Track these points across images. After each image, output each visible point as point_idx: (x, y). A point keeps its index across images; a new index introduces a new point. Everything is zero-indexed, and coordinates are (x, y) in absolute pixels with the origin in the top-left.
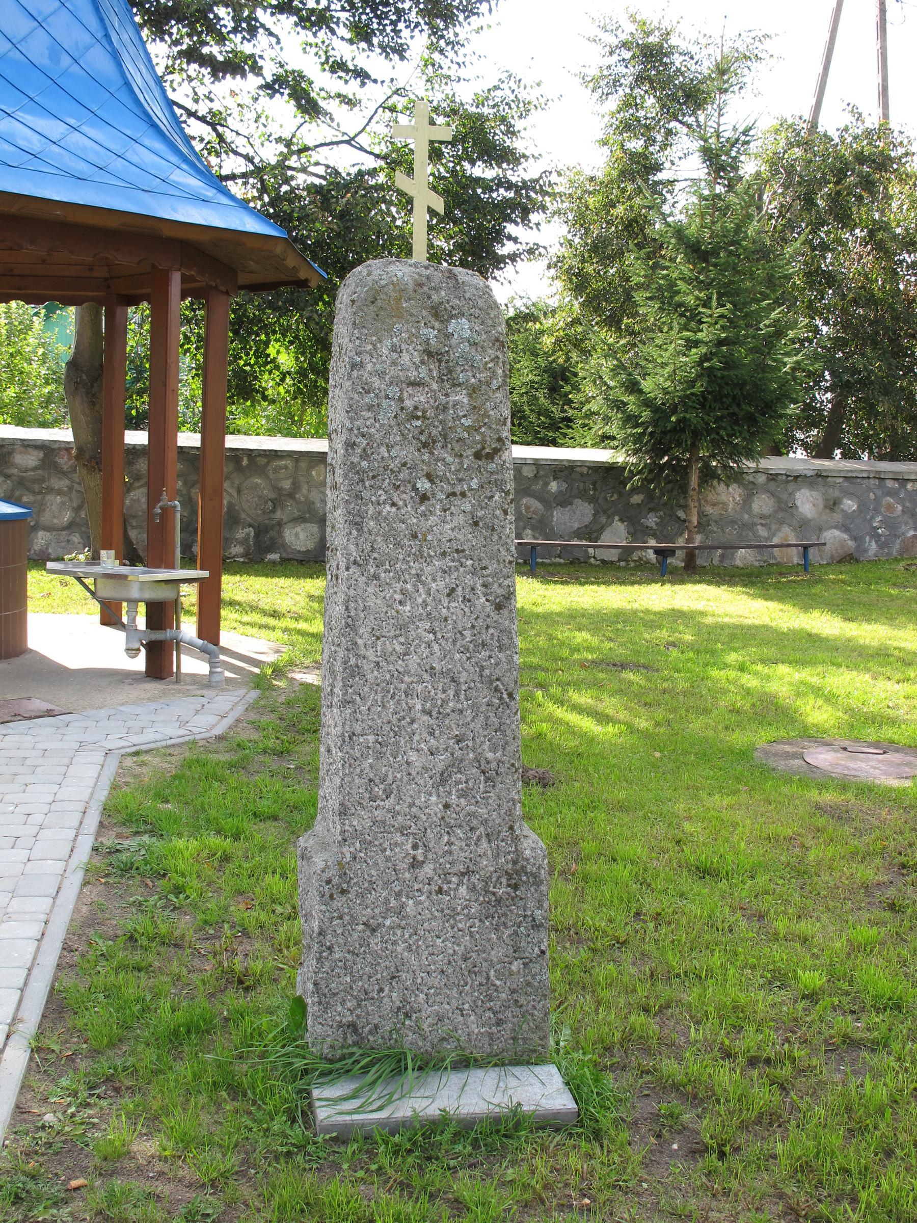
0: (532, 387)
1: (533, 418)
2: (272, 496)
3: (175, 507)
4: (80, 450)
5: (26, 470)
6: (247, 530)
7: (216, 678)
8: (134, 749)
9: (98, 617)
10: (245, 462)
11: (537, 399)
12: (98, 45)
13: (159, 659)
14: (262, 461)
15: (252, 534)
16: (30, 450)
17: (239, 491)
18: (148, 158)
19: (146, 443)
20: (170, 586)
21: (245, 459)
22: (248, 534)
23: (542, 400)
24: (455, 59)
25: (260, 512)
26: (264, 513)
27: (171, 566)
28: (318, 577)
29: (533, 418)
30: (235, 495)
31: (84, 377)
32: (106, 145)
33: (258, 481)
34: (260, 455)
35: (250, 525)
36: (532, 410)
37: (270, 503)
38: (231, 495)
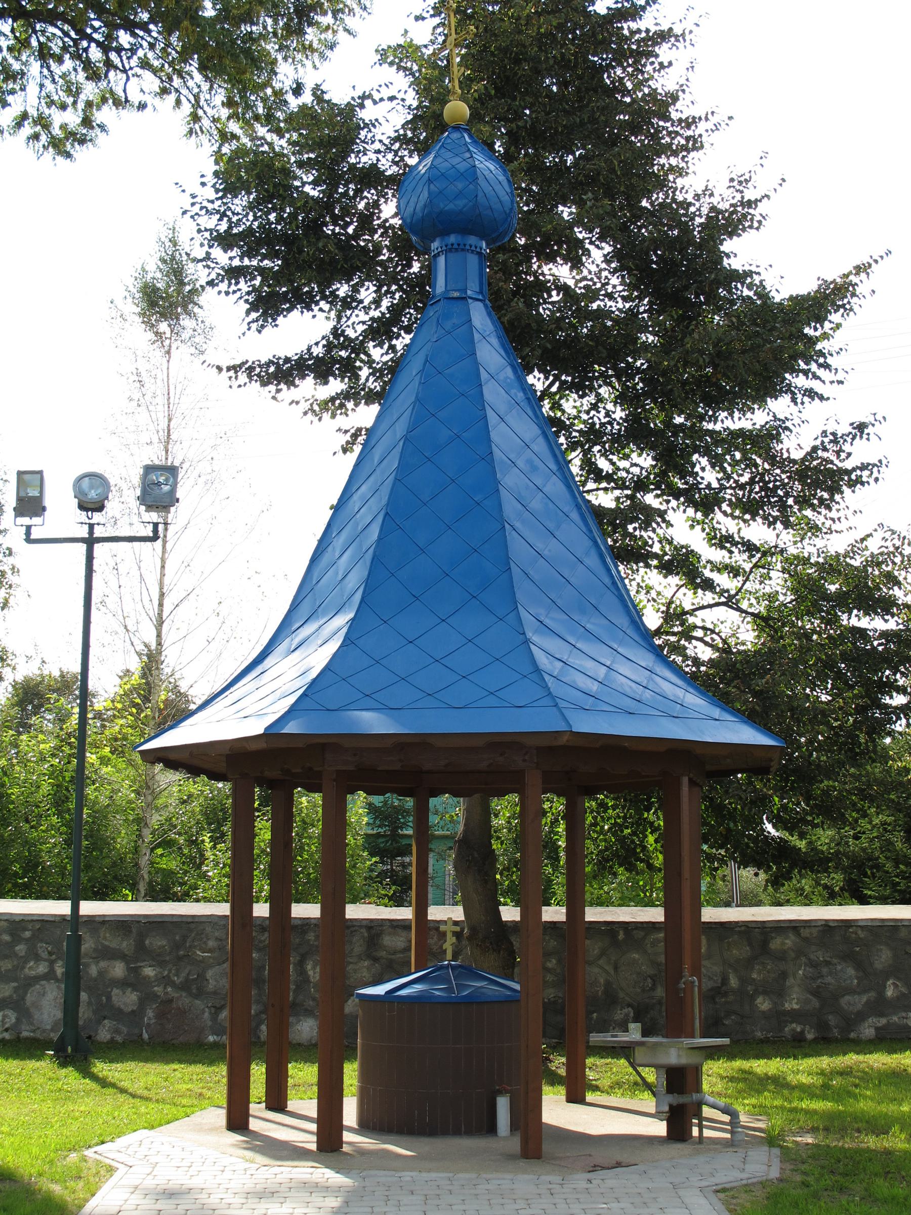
0: (885, 829)
1: (889, 866)
2: (651, 972)
3: (693, 982)
4: (473, 929)
5: (395, 953)
6: (626, 1010)
7: (738, 1137)
8: (719, 1187)
9: (564, 1098)
10: (621, 936)
11: (892, 844)
12: (609, 592)
13: (680, 1121)
14: (639, 934)
15: (632, 1014)
16: (399, 931)
17: (616, 968)
18: (667, 688)
19: (518, 919)
20: (696, 1051)
21: (621, 933)
22: (627, 1015)
23: (899, 845)
24: (829, 515)
25: (639, 990)
26: (643, 991)
27: (693, 1037)
28: (719, 1059)
29: (889, 866)
30: (612, 972)
31: (476, 855)
32: (632, 678)
33: (636, 956)
34: (636, 928)
35: (629, 1005)
36: (887, 858)
37: (649, 980)
38: (608, 973)
